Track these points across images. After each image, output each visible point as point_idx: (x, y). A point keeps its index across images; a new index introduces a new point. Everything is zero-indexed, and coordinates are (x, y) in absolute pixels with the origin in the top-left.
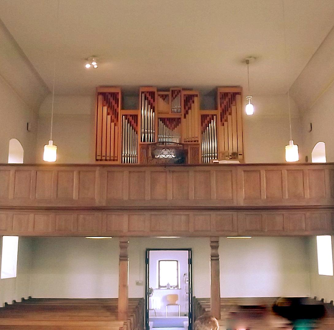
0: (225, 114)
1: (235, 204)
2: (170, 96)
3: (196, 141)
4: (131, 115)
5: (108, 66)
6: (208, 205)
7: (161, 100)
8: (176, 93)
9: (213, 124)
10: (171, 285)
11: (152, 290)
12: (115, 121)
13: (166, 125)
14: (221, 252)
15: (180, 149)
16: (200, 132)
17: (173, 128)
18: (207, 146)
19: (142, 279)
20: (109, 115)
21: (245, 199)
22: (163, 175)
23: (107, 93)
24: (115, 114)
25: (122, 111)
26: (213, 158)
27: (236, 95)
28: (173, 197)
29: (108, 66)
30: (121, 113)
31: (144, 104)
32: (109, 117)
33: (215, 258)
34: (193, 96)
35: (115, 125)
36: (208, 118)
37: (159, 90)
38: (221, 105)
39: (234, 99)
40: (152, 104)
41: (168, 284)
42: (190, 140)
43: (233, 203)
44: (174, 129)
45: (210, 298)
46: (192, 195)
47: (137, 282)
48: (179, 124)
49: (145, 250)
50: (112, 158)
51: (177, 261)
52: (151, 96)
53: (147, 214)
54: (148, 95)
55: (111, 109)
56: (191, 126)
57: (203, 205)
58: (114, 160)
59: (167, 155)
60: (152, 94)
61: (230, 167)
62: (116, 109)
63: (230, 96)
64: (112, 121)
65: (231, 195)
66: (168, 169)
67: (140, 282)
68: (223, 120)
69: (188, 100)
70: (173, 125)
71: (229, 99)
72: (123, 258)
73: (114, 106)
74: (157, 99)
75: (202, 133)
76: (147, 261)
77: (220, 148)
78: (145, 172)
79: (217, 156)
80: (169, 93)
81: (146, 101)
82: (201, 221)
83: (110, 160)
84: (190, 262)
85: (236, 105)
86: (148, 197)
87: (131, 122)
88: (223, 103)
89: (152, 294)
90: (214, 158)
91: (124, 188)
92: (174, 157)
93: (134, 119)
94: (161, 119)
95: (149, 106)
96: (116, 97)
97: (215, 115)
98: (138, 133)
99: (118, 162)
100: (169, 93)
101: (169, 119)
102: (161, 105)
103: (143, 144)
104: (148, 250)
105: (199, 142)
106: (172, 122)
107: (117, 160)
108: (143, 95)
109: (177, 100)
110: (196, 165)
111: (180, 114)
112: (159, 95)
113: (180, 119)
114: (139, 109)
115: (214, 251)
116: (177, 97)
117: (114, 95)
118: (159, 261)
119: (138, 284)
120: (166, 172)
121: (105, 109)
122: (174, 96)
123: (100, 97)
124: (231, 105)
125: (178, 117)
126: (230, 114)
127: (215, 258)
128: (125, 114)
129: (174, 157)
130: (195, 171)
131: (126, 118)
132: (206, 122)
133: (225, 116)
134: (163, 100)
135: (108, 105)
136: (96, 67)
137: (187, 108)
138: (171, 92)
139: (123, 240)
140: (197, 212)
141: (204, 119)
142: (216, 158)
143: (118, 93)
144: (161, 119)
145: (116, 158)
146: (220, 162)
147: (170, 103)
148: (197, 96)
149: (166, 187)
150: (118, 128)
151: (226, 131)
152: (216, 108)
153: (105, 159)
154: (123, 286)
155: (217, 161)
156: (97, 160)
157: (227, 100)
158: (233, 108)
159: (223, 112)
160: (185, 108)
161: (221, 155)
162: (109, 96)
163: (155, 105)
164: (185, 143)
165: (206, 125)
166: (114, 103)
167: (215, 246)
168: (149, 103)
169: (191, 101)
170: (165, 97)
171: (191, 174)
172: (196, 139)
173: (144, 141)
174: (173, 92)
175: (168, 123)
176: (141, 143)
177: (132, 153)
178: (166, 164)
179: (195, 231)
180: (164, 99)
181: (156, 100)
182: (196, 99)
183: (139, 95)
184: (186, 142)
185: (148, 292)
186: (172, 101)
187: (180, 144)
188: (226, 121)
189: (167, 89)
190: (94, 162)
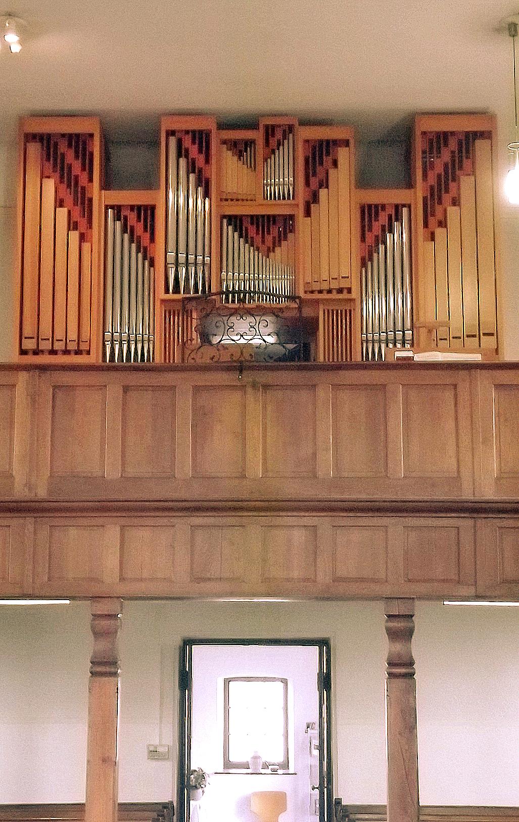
0: (440, 203)
1: (467, 494)
2: (260, 143)
3: (345, 291)
4: (132, 208)
5: (54, 46)
6: (376, 497)
7: (229, 160)
8: (279, 135)
9: (398, 238)
10: (266, 758)
11: (202, 776)
12: (83, 227)
13: (247, 236)
14: (420, 649)
15: (286, 315)
16: (356, 263)
17: (269, 249)
18: (378, 309)
19: (168, 738)
20: (61, 206)
21: (498, 479)
22: (236, 396)
23: (55, 135)
24: (83, 203)
25: (103, 192)
26: (391, 346)
27: (474, 140)
28: (265, 470)
29: (54, 46)
30: (100, 200)
31: (174, 169)
32: (63, 212)
33: (402, 670)
34: (336, 143)
35: (82, 238)
36: (383, 219)
37: (223, 126)
38: (425, 175)
39: (468, 152)
40: (200, 171)
41: (256, 758)
42: (325, 286)
43: (460, 488)
44: (270, 250)
45: (385, 806)
46: (326, 466)
47: (152, 749)
48: (290, 236)
49: (178, 642)
50: (72, 346)
51: (285, 682)
52: (197, 142)
53: (182, 524)
54: (187, 142)
55: (69, 186)
56: (329, 240)
57: (364, 496)
58: (78, 352)
59: (255, 334)
60: (202, 139)
61: (450, 372)
62: (83, 188)
63: (453, 144)
64: (72, 225)
65: (450, 463)
66: (248, 377)
67: (160, 749)
68: (432, 221)
69: (320, 156)
70: (269, 239)
71: (453, 152)
72: (104, 667)
73: (77, 177)
74: (219, 152)
75: (364, 264)
76: (185, 680)
77: (421, 314)
78: (173, 388)
79: (410, 338)
80: (256, 134)
81: (183, 161)
82: (355, 547)
83: (66, 352)
84: (325, 682)
85: (474, 173)
86: (185, 468)
87: (132, 228)
88: (432, 167)
89: (200, 790)
90: (395, 345)
91: (104, 442)
92: (271, 340)
93: (142, 221)
94: (236, 221)
95: (192, 177)
96: (84, 149)
97: (404, 206)
98: (156, 264)
99: (93, 358)
100: (258, 136)
101: (254, 219)
102: (232, 173)
103: (174, 301)
104: (189, 642)
105: (355, 294)
106: (264, 229)
107: (88, 353)
108: (173, 141)
109: (283, 156)
110: (338, 368)
111: (291, 201)
112: (224, 142)
113: (292, 217)
114: (158, 188)
115: (398, 647)
116: (281, 148)
117: (79, 142)
118: (227, 682)
119: (154, 754)
120: (243, 388)
121: (50, 185)
122: (273, 142)
123: (34, 149)
124: (458, 172)
125: (287, 211)
126: (455, 202)
127: (402, 670)
128: (111, 204)
129: (271, 340)
130: (336, 387)
131: (117, 217)
132: (377, 226)
133: (439, 209)
134: (236, 158)
135: (58, 175)
136: (16, 48)
137: (314, 181)
138: (262, 130)
139: (103, 608)
140: (344, 520)
141: (370, 221)
142: (399, 346)
143: (91, 135)
144: (236, 221)
145: (84, 347)
146: (419, 358)
147: (260, 167)
148: (347, 143)
149: (242, 437)
150: (93, 251)
151: (442, 259)
152: (410, 185)
153: (64, 348)
154: (103, 760)
155: (410, 354)
156: (23, 352)
157: (446, 156)
158: (466, 183)
159: (432, 195)
160: (307, 183)
161: (423, 331)
162: (63, 147)
163: (212, 172)
164: (309, 296)
165: (377, 237)
166: (77, 168)
167: (401, 630)
168: (192, 167)
169: (327, 161)
170: (275, 147)
171: (324, 393)
172: (344, 284)
173: (176, 290)
174: (270, 131)
175: (252, 231)
176: (167, 297)
177: (137, 326)
178: (244, 364)
179: (337, 580)
180: (240, 155)
181: (213, 161)
182: (343, 155)
183: (157, 144)
184: (312, 292)
185: (188, 783)
186: (265, 160)
187: (292, 298)
188: (442, 224)
189: (250, 123)
190: (14, 358)
